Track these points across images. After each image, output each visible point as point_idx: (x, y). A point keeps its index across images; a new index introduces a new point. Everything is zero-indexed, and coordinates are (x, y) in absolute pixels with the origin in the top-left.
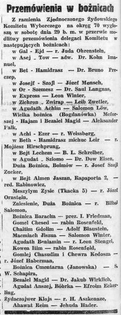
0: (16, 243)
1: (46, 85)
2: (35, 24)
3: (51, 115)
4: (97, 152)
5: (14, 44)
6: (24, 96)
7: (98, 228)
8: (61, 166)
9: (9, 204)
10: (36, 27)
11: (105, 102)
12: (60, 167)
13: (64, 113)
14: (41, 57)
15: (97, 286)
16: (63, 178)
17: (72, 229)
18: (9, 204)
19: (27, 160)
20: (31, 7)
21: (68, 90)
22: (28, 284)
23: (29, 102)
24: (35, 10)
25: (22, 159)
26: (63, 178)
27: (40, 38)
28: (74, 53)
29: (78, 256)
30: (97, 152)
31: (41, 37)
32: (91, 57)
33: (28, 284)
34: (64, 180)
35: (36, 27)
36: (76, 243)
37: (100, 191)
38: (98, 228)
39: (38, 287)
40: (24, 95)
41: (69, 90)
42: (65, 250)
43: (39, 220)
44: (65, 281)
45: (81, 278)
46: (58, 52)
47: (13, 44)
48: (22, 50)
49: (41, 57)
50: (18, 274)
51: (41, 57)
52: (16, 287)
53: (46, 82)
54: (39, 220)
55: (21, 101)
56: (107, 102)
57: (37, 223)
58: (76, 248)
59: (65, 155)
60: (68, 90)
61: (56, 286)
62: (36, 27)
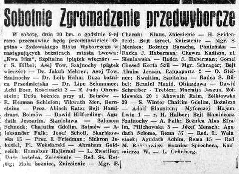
0: (110, 116)
1: (166, 80)
2: (85, 45)
3: (186, 78)
5: (15, 52)
8: (68, 164)
10: (85, 48)
13: (91, 107)
14: (57, 65)
16: (221, 53)
17: (64, 127)
19: (149, 140)
21: (41, 72)
25: (109, 115)
26: (221, 53)
27: (20, 71)
29: (192, 54)
31: (38, 114)
34: (10, 80)
35: (85, 48)
36: (156, 116)
39: (145, 140)
41: (43, 73)
42: (117, 123)
44: (43, 73)
45: (59, 70)
46: (49, 79)
47: (13, 52)
48: (174, 150)
49: (109, 70)
51: (57, 65)
52: (110, 116)
53: (74, 64)
55: (91, 101)
58: (217, 121)
60: (41, 72)
62: (86, 48)
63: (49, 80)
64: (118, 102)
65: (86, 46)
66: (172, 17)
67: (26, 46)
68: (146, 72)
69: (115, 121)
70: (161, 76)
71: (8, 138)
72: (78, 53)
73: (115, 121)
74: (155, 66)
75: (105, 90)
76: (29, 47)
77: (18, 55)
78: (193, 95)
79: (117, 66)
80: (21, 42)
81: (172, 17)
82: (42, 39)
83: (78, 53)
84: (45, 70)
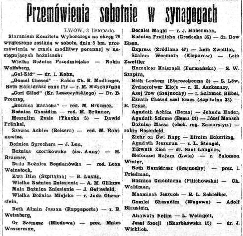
4: (22, 215)
6: (136, 50)
7: (139, 207)
9: (8, 164)
11: (160, 87)
12: (218, 196)
15: (199, 216)
18: (8, 164)
20: (41, 8)
22: (218, 97)
23: (138, 215)
24: (31, 15)
28: (223, 102)
30: (22, 215)
32: (42, 118)
33: (218, 97)
35: (66, 37)
37: (124, 131)
38: (139, 207)
40: (136, 49)
43: (40, 109)
44: (111, 94)
50: (177, 94)
54: (40, 109)
56: (233, 50)
57: (39, 112)
59: (79, 178)
61: (203, 125)
63: (112, 95)
64: (119, 50)
65: (67, 36)
66: (76, 15)
67: (132, 86)
68: (48, 209)
69: (116, 87)
70: (144, 83)
71: (103, 35)
72: (5, 49)
73: (116, 87)
74: (22, 165)
75: (108, 196)
76: (135, 87)
77: (64, 48)
78: (111, 130)
79: (177, 50)
80: (92, 224)
81: (76, 15)
82: (116, 117)
83: (5, 49)
84: (112, 105)
